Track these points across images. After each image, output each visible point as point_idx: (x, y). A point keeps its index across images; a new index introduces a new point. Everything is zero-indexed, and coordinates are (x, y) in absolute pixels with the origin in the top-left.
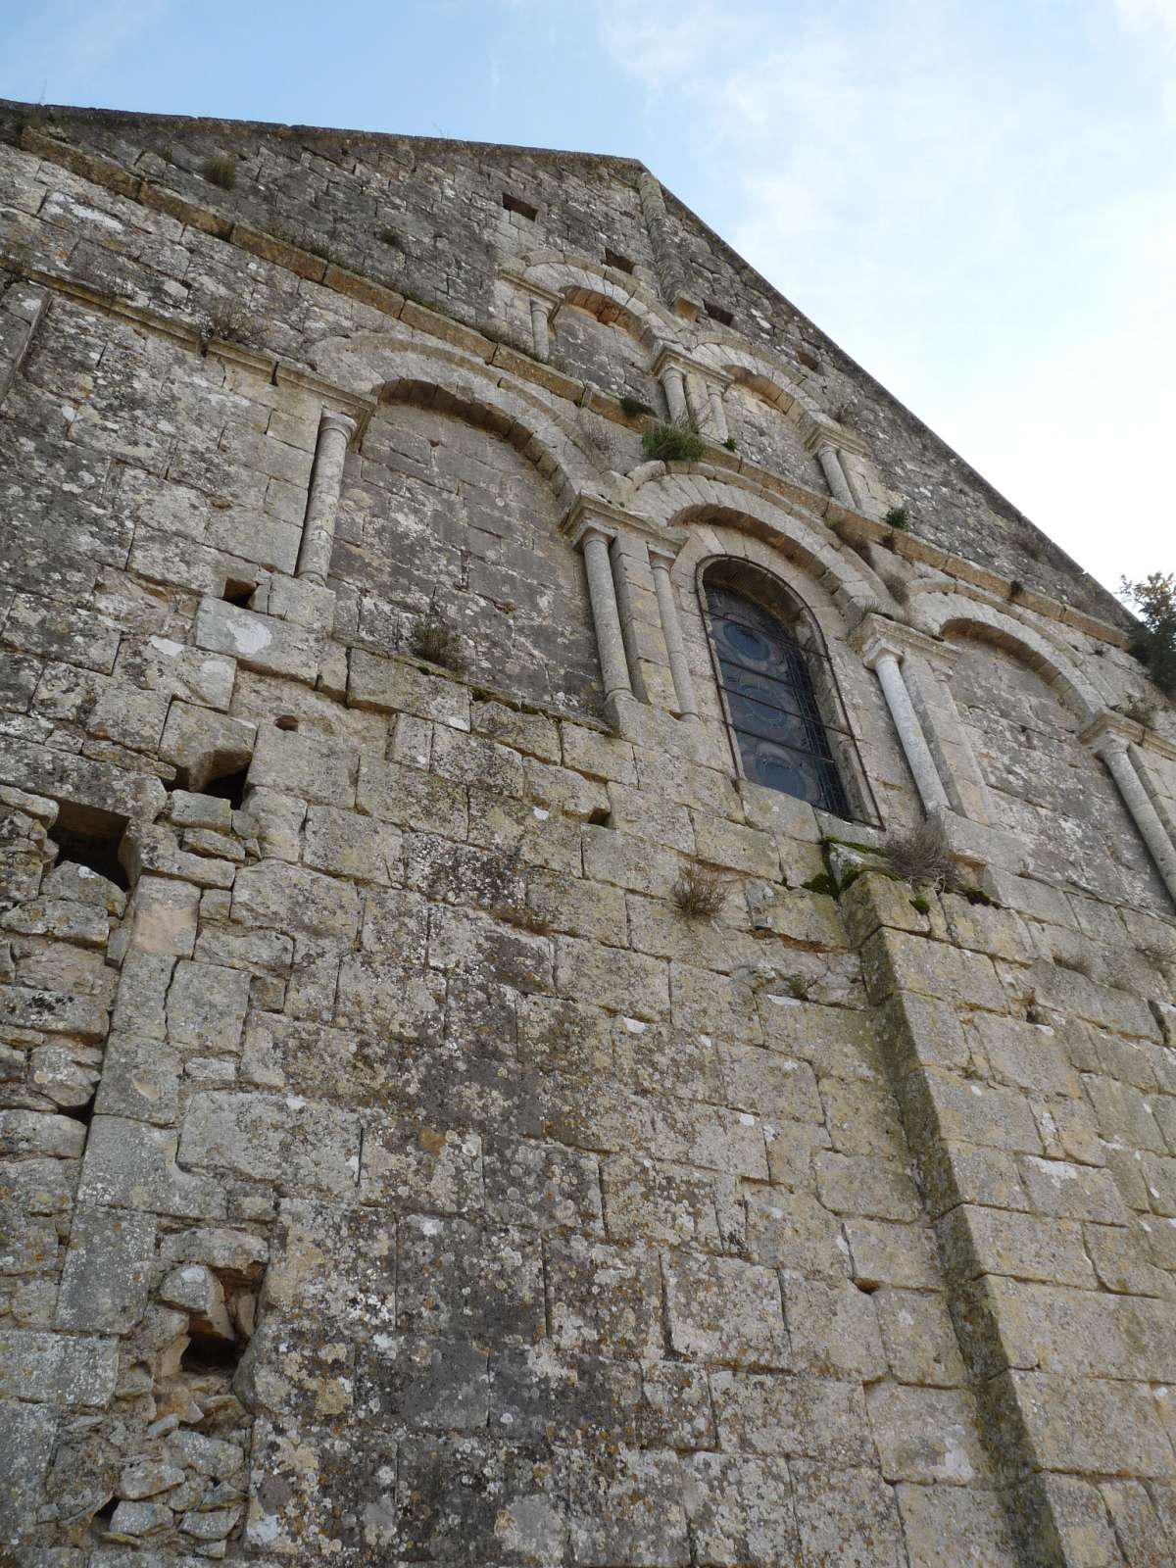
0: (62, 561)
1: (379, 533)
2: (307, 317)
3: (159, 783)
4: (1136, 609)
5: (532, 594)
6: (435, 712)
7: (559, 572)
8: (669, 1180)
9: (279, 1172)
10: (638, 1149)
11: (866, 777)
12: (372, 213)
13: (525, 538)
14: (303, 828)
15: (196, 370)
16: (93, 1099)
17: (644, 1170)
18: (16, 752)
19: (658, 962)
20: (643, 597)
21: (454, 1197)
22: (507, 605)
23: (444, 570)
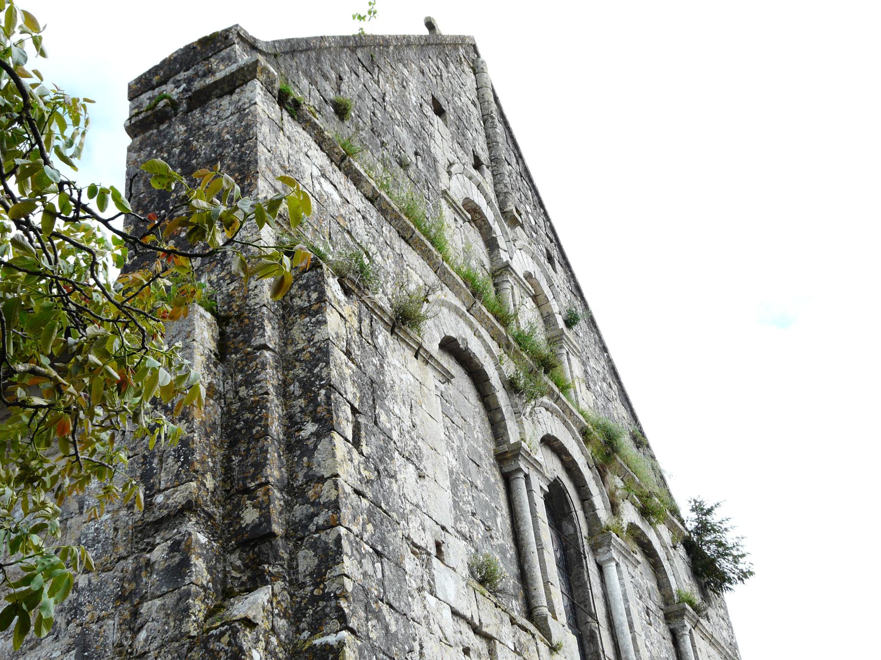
4: (686, 513)
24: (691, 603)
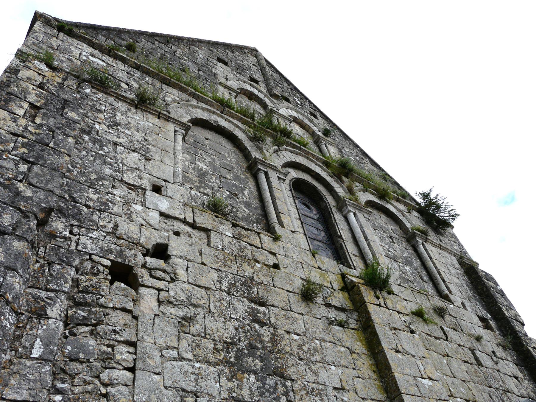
0: (101, 178)
1: (194, 169)
2: (165, 96)
3: (141, 254)
4: (419, 200)
5: (243, 190)
6: (221, 230)
7: (249, 183)
8: (313, 389)
9: (196, 389)
10: (302, 379)
11: (348, 253)
12: (178, 62)
13: (237, 171)
14: (187, 270)
15: (135, 113)
17: (305, 386)
18: (95, 244)
19: (299, 315)
20: (278, 192)
21: (250, 396)
22: (235, 194)
23: (215, 181)
24: (419, 230)
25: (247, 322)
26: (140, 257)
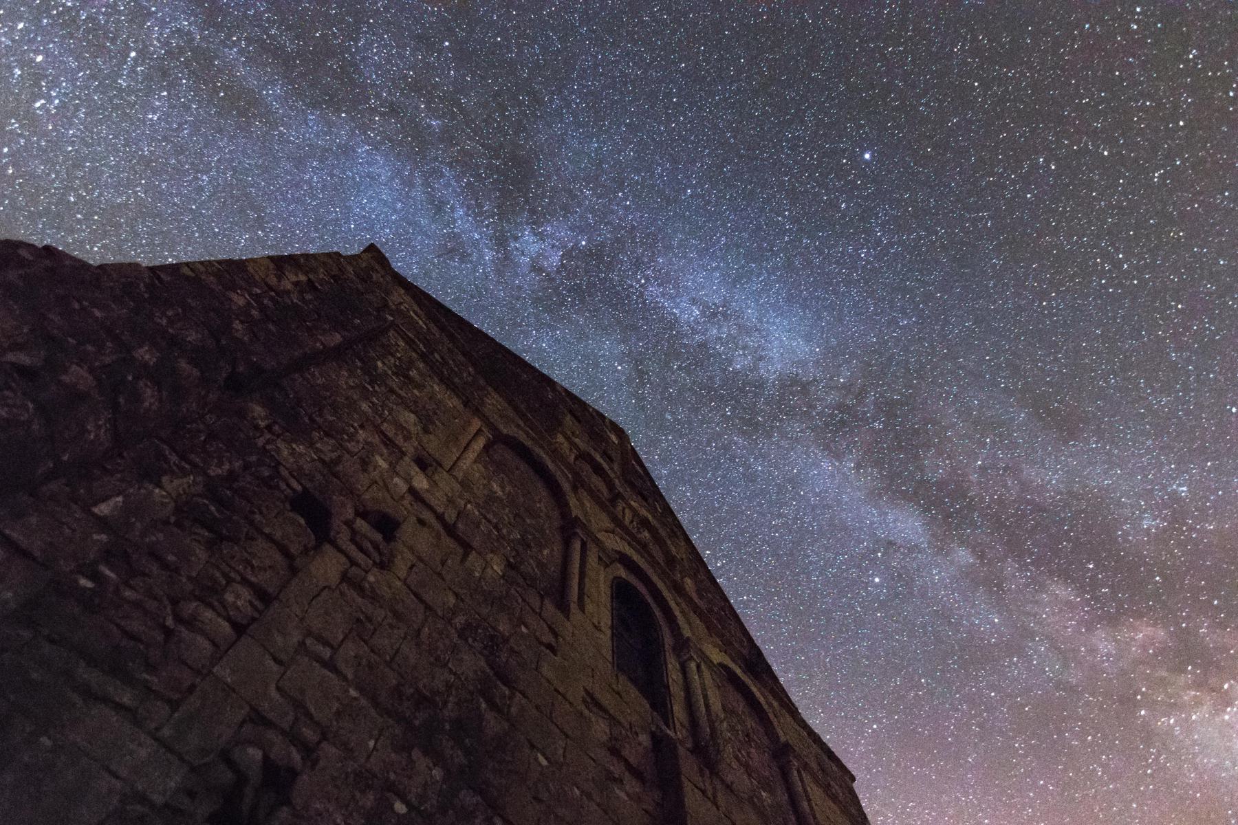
14: (411, 568)
16: (249, 625)
25: (471, 688)
26: (349, 513)
